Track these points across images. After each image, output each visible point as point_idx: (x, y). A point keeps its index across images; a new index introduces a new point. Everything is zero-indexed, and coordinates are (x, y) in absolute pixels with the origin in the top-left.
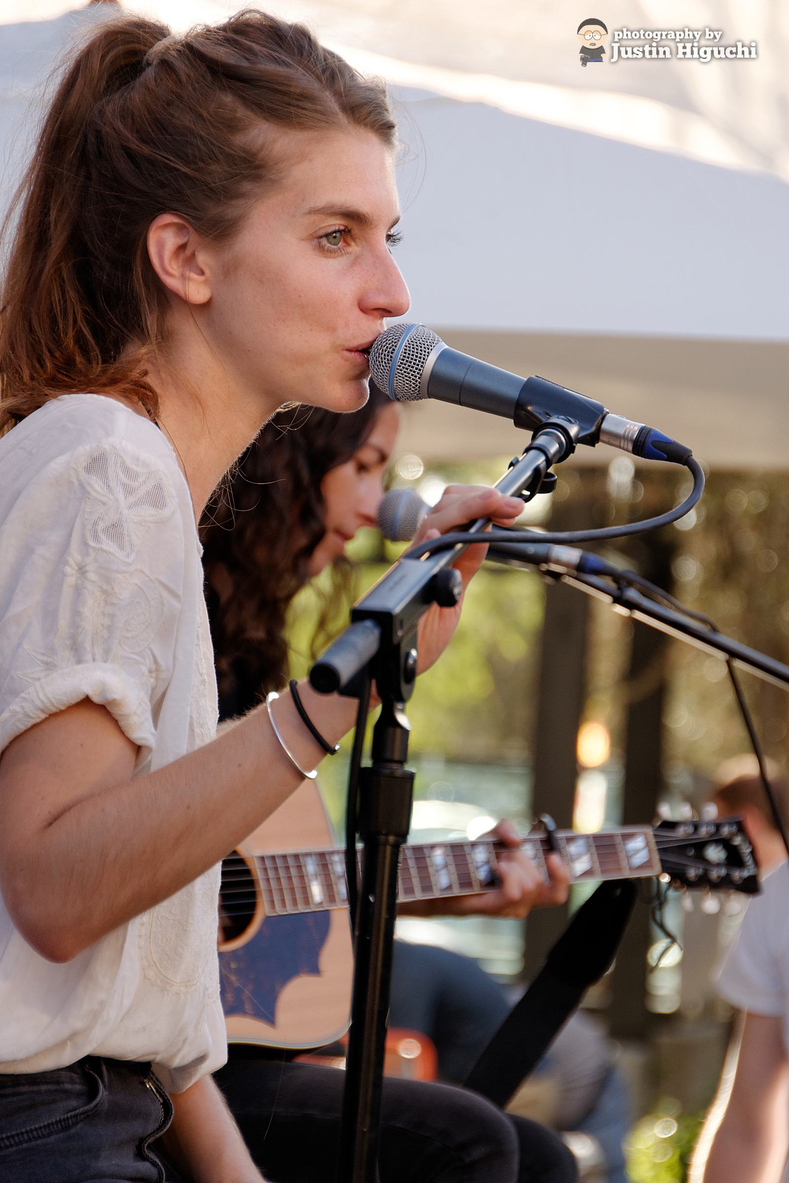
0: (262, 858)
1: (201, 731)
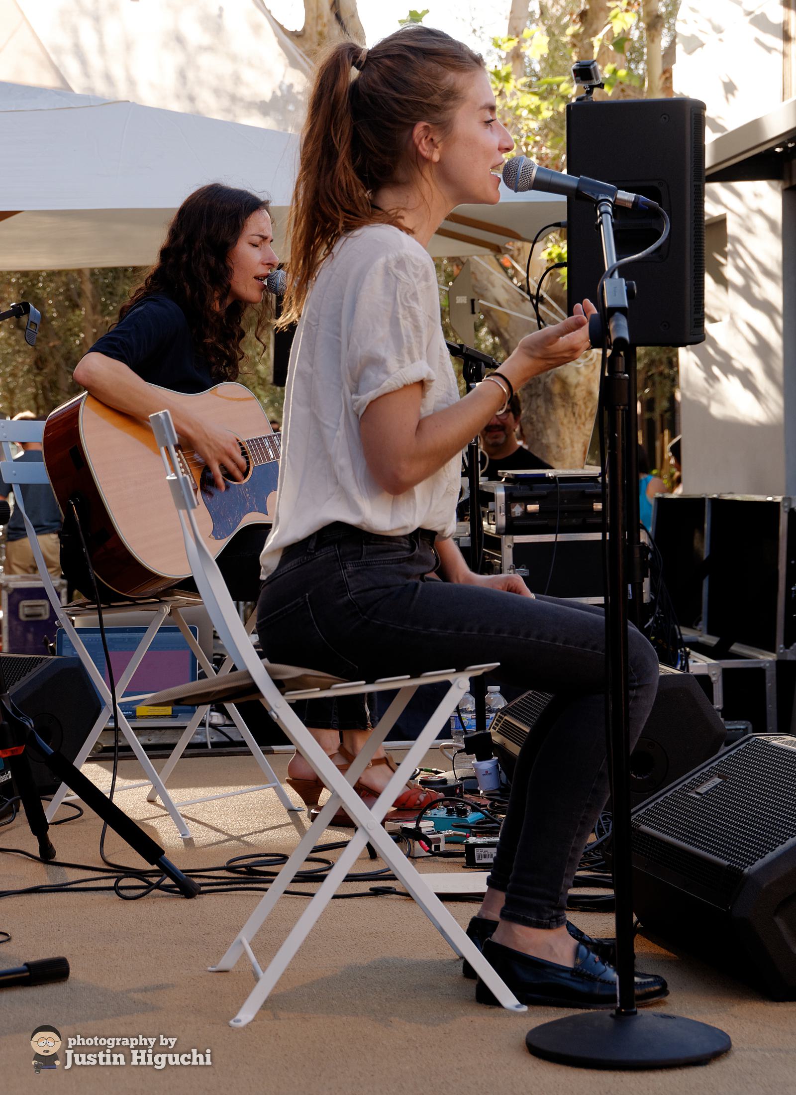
0: (248, 441)
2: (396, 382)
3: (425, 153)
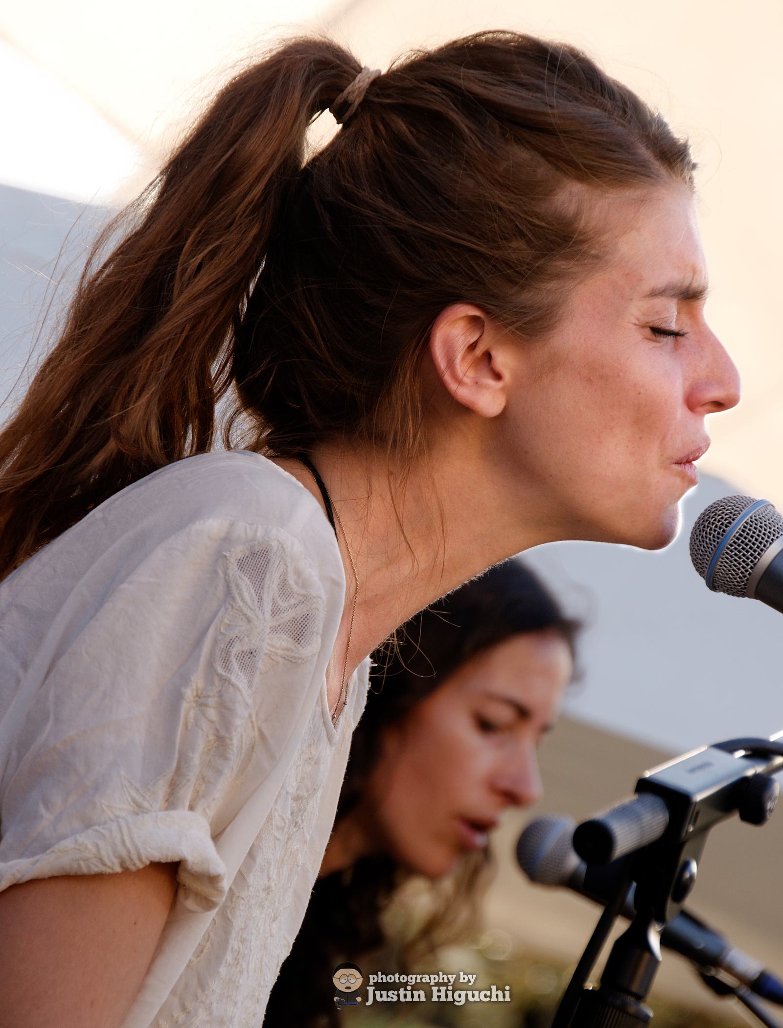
1: (239, 948)
2: (97, 846)
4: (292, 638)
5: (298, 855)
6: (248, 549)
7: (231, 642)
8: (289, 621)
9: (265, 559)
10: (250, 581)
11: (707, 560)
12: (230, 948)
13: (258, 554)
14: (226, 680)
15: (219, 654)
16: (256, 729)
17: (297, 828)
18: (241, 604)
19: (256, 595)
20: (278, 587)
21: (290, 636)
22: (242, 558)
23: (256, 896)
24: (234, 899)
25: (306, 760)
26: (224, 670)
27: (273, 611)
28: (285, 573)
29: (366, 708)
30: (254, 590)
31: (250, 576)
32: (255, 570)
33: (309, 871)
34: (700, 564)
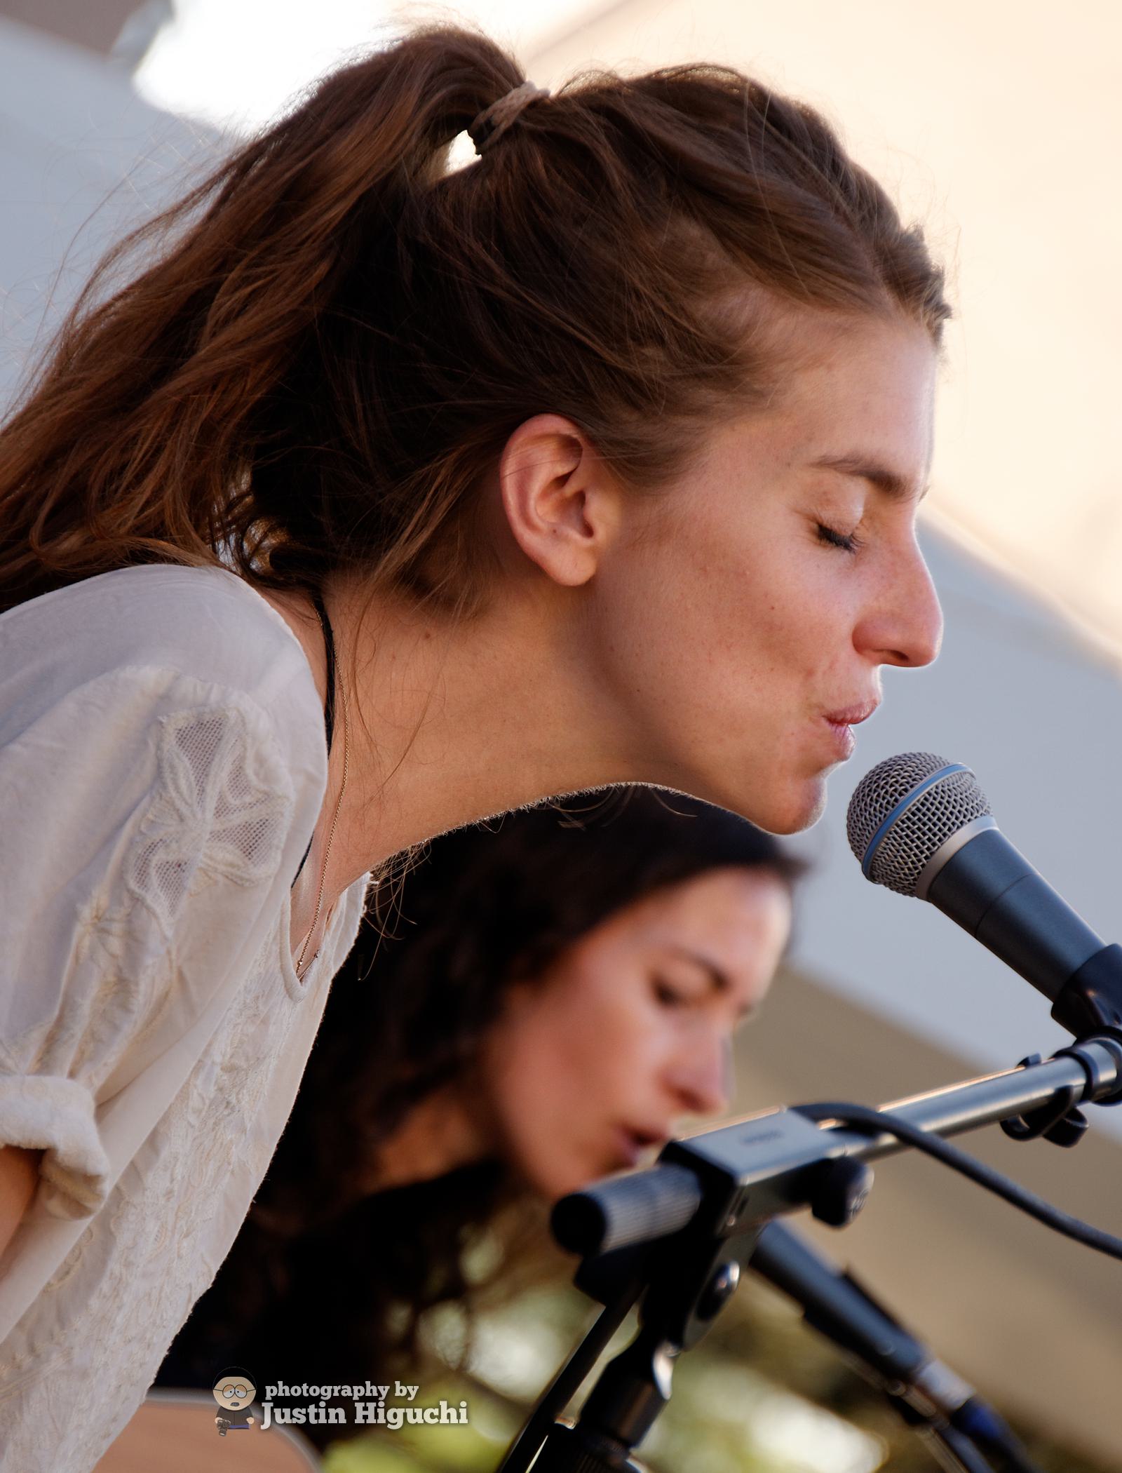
1: (121, 1274)
3: (531, 540)
4: (241, 850)
5: (231, 1148)
6: (194, 717)
7: (153, 846)
8: (239, 826)
9: (216, 735)
10: (191, 764)
11: (867, 837)
12: (108, 1273)
13: (208, 726)
14: (138, 899)
15: (134, 861)
16: (175, 970)
17: (230, 1111)
18: (174, 794)
19: (197, 785)
20: (228, 776)
21: (239, 847)
22: (184, 728)
23: (154, 1203)
24: (122, 1205)
25: (249, 1018)
26: (138, 885)
27: (218, 810)
28: (242, 759)
29: (357, 941)
30: (194, 776)
31: (191, 755)
32: (200, 749)
33: (250, 1172)
34: (858, 841)
